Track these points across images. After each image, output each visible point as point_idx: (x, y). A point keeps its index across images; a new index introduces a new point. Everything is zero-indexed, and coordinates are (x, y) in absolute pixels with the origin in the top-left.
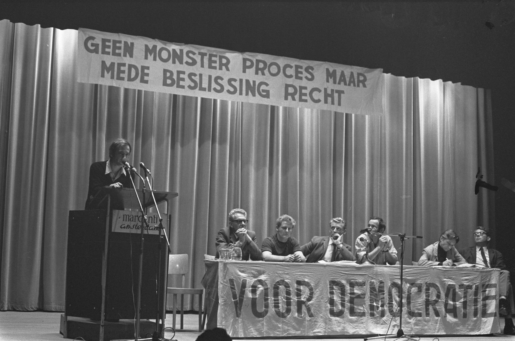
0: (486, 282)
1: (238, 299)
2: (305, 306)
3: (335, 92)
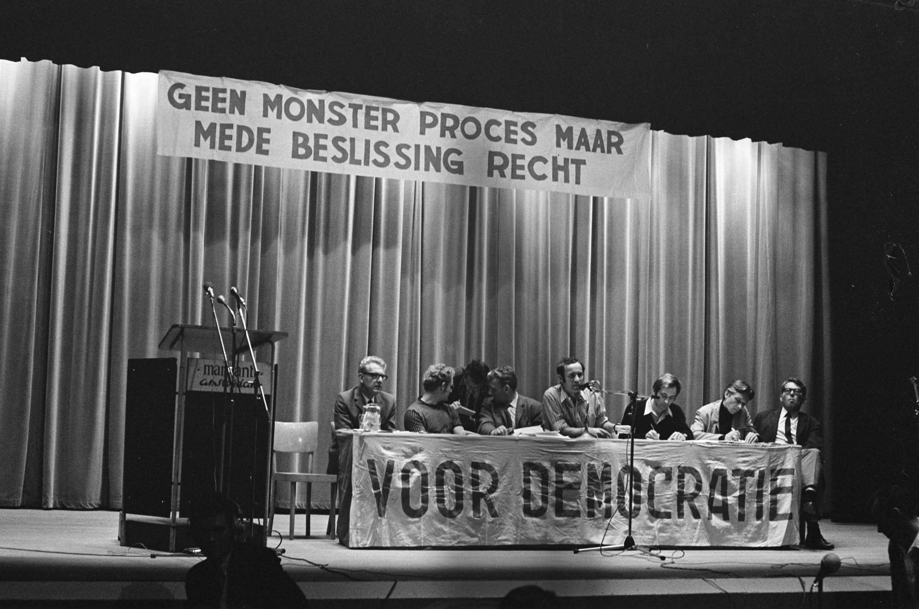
0: (777, 465)
1: (381, 489)
2: (485, 500)
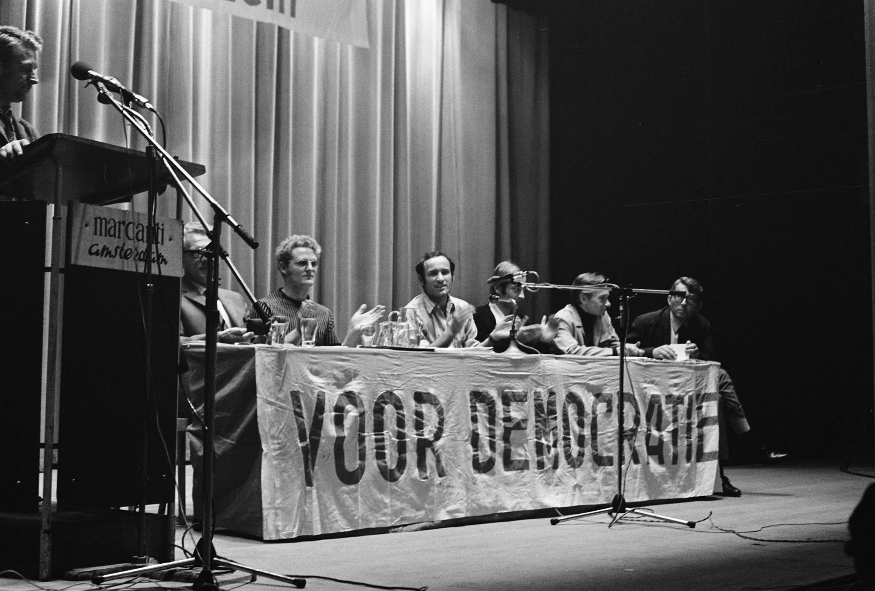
2: (433, 450)
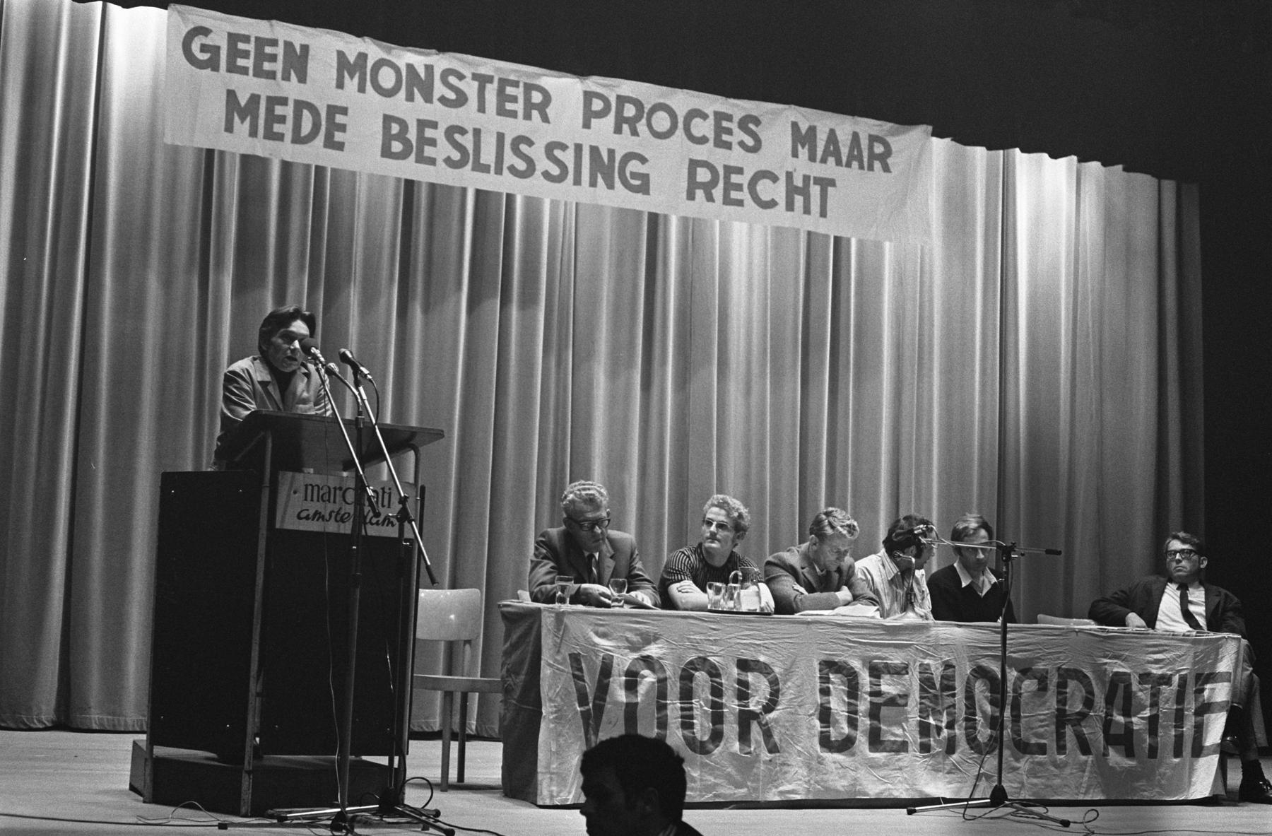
1: (591, 705)
2: (759, 723)
3: (812, 182)
